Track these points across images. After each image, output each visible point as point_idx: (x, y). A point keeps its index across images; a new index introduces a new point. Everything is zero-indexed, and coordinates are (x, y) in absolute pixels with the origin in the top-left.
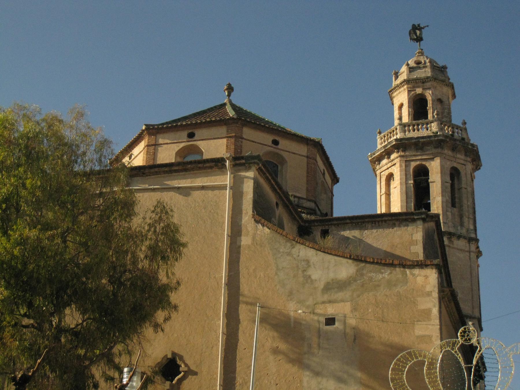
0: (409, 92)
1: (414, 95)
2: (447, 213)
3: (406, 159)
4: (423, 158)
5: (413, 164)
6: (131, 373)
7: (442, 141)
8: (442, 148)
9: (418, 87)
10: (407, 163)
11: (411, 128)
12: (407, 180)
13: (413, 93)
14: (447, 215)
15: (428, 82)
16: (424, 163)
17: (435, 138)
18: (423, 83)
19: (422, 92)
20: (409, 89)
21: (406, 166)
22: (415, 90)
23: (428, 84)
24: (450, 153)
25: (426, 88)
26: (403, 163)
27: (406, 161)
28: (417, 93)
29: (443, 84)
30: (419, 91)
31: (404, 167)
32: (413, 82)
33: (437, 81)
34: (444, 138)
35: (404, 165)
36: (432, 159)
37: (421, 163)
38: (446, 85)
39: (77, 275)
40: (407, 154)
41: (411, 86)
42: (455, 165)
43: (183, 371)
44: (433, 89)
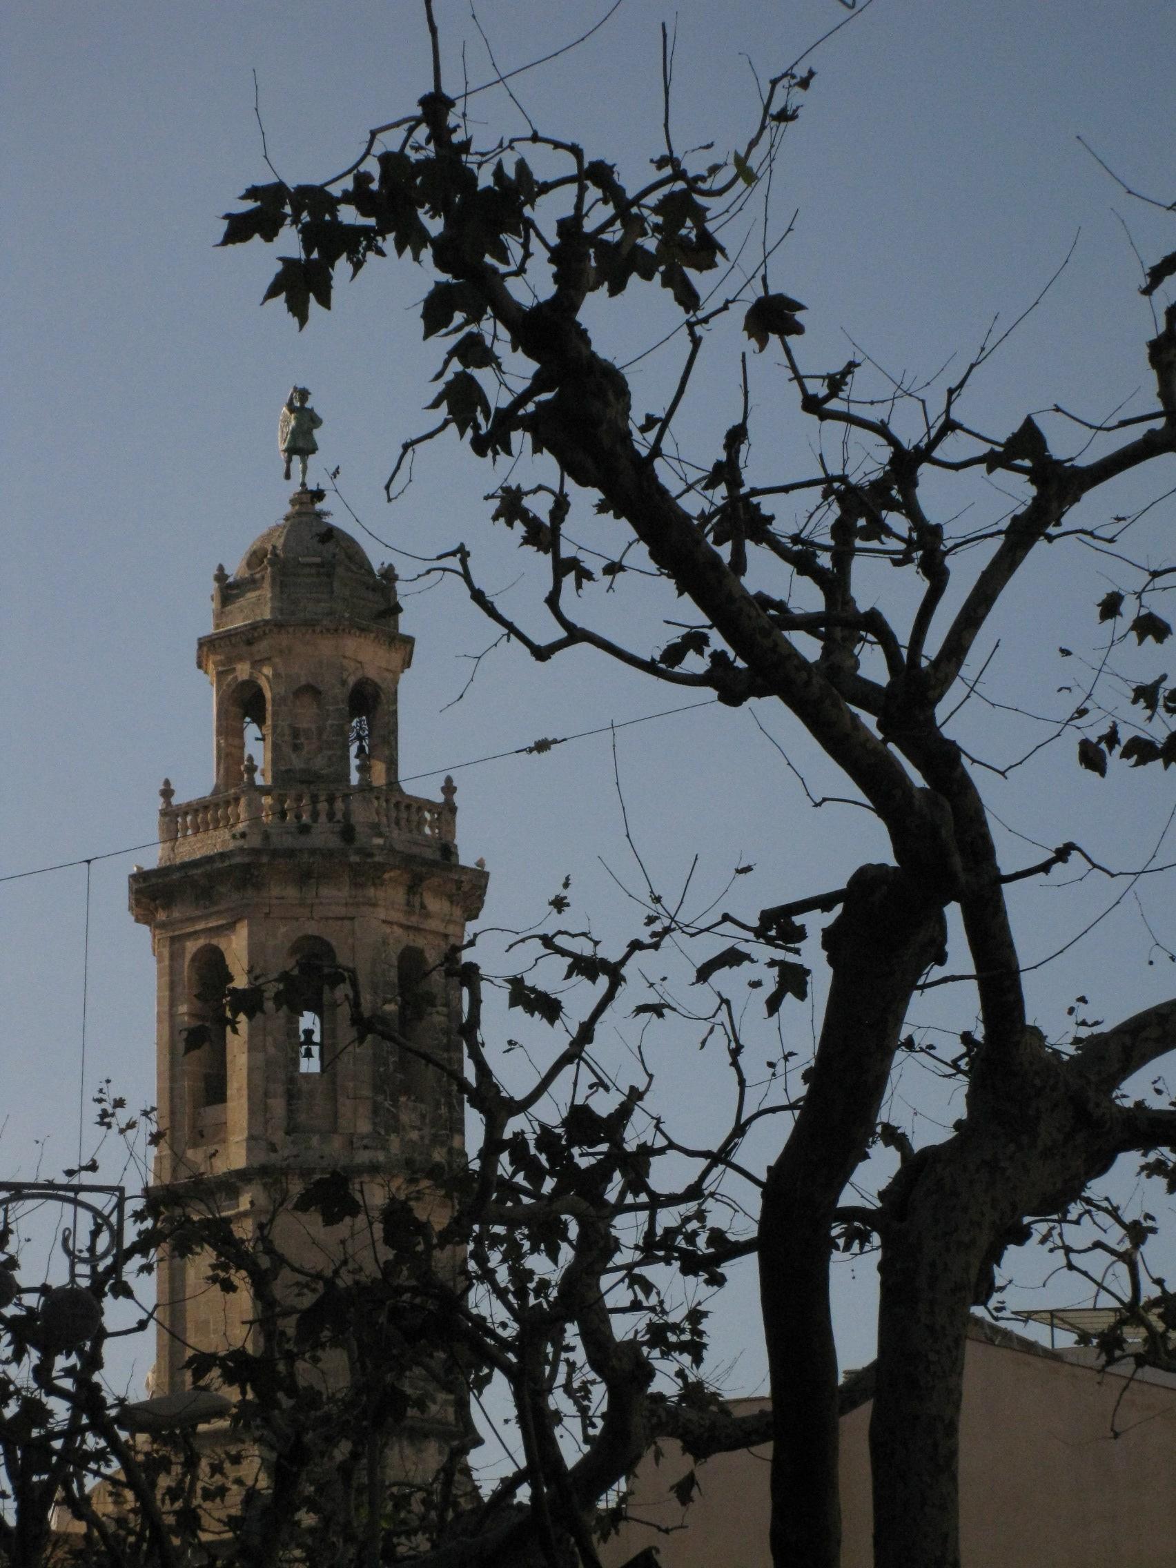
0: (220, 675)
1: (233, 687)
2: (269, 1101)
3: (171, 934)
4: (210, 925)
5: (192, 947)
6: (362, 1511)
7: (247, 868)
8: (258, 887)
9: (240, 659)
10: (177, 946)
11: (189, 818)
12: (173, 1004)
13: (230, 677)
14: (266, 1109)
15: (260, 638)
16: (214, 942)
17: (223, 862)
18: (249, 643)
19: (251, 674)
20: (220, 669)
21: (173, 957)
22: (234, 669)
23: (263, 646)
24: (291, 892)
25: (260, 661)
26: (164, 946)
27: (173, 939)
28: (240, 679)
29: (314, 631)
30: (243, 671)
31: (167, 962)
32: (222, 644)
33: (291, 630)
34: (247, 860)
35: (166, 952)
36: (231, 926)
37: (207, 942)
38: (328, 630)
39: (464, 878)
40: (176, 915)
41: (223, 658)
42: (312, 928)
43: (1095, 1336)
44: (277, 660)
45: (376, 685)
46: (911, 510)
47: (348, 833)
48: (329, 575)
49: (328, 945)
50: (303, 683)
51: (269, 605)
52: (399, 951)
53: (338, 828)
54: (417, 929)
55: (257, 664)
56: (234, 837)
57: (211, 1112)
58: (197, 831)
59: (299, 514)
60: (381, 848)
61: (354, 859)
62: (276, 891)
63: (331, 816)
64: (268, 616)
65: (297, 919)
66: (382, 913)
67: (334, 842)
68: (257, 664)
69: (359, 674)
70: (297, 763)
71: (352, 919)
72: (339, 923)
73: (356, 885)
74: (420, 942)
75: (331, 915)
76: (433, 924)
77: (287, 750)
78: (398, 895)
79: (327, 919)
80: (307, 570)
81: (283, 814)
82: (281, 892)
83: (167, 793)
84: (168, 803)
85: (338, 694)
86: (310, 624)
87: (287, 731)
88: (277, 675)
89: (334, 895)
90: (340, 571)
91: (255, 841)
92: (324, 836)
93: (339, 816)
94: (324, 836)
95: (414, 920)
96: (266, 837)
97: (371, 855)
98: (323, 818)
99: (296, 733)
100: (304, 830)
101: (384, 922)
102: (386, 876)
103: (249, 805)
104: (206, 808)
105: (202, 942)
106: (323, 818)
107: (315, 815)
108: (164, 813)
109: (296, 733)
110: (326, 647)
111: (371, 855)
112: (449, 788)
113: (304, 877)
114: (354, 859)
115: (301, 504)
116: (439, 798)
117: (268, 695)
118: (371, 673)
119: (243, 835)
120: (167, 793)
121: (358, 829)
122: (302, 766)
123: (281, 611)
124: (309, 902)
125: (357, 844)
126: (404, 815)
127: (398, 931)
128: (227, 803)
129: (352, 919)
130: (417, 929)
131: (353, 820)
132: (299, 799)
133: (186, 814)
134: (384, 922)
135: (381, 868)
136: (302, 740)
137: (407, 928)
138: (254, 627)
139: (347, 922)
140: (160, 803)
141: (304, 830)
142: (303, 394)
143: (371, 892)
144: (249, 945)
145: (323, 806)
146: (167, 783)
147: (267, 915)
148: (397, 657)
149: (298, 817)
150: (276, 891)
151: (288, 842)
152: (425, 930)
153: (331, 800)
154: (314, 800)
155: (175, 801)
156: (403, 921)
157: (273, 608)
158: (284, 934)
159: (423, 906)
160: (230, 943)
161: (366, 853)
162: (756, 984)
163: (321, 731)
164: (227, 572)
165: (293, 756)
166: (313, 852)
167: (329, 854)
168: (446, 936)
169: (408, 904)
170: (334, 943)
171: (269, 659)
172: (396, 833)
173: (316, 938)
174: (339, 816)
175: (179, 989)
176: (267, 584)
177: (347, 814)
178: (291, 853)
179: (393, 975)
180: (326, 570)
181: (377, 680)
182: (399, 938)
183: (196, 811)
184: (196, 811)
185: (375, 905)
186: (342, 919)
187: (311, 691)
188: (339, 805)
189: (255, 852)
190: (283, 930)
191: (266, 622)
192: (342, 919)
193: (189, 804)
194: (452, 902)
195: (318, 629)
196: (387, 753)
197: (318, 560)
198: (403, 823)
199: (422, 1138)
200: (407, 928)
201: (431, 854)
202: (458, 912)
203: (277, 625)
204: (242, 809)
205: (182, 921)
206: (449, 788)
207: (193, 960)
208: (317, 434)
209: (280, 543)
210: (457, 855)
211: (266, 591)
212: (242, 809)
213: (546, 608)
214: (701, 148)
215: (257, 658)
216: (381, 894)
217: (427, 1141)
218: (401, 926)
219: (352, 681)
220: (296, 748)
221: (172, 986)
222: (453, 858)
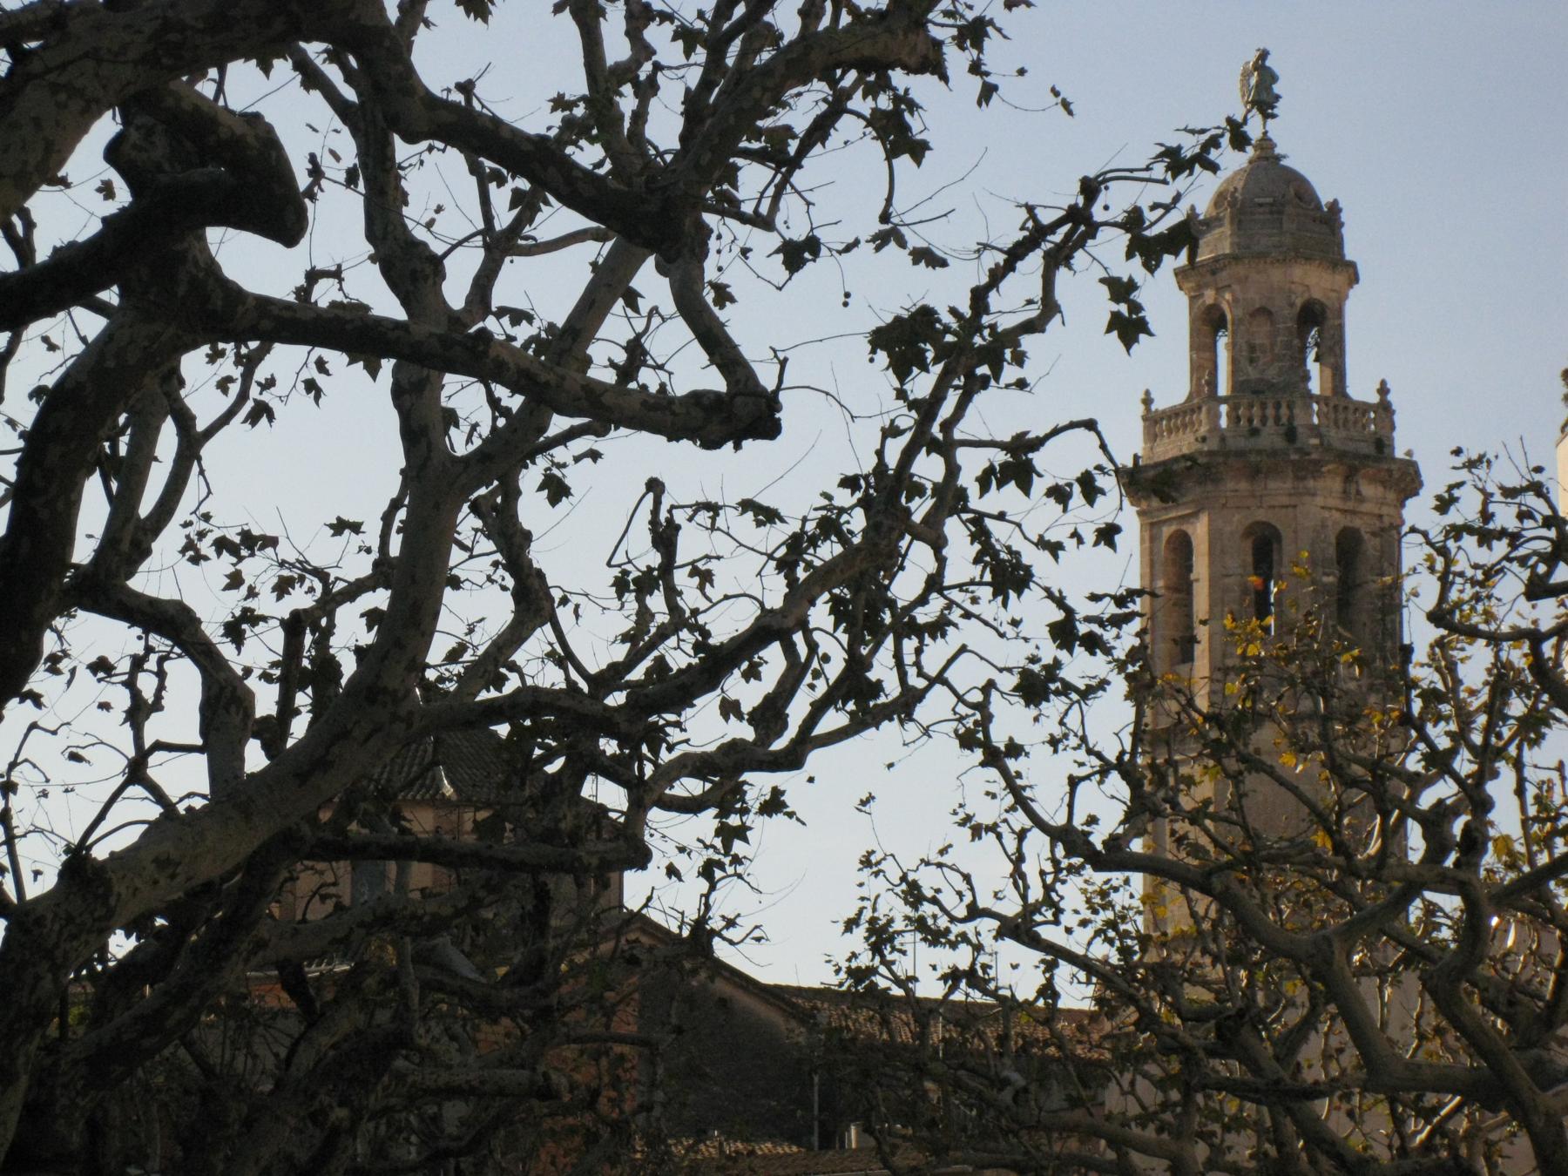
5: (1167, 531)
7: (1208, 467)
9: (1207, 286)
10: (1155, 531)
13: (1201, 301)
16: (1184, 527)
18: (1214, 273)
23: (1224, 276)
24: (1244, 486)
27: (1152, 525)
30: (1209, 296)
36: (1195, 515)
42: (1261, 515)
44: (1236, 287)
45: (1322, 304)
46: (792, 582)
47: (1291, 435)
48: (1280, 213)
49: (1274, 528)
50: (1257, 306)
51: (1229, 240)
52: (1337, 531)
53: (1282, 430)
54: (1354, 512)
55: (1219, 290)
56: (1197, 440)
57: (1183, 669)
58: (1170, 432)
59: (1259, 158)
60: (1316, 447)
61: (1294, 457)
62: (1230, 485)
63: (1277, 419)
64: (1227, 251)
65: (1248, 508)
66: (1319, 501)
67: (1280, 443)
68: (1219, 290)
69: (1306, 296)
70: (1252, 373)
71: (1295, 506)
72: (1284, 510)
73: (1299, 478)
74: (1357, 522)
75: (1276, 503)
76: (1366, 507)
77: (1244, 363)
78: (1336, 484)
79: (1274, 507)
80: (1261, 210)
81: (1238, 419)
82: (1235, 486)
83: (1147, 401)
84: (1148, 409)
85: (1287, 316)
86: (1262, 255)
87: (1245, 347)
88: (1235, 300)
89: (1279, 488)
90: (1289, 209)
91: (1213, 444)
92: (1271, 437)
93: (1284, 420)
94: (1271, 437)
95: (1350, 505)
96: (1223, 439)
97: (1308, 454)
98: (1270, 422)
99: (1252, 348)
100: (1254, 432)
101: (1323, 508)
102: (1324, 469)
103: (1209, 412)
104: (1185, 413)
105: (1173, 528)
106: (1270, 422)
107: (1264, 420)
108: (1145, 418)
109: (1252, 348)
110: (1277, 275)
111: (1308, 454)
112: (1383, 390)
113: (1254, 473)
114: (1294, 457)
115: (1262, 149)
116: (1374, 399)
117: (1229, 317)
118: (1317, 294)
119: (1204, 439)
120: (1147, 401)
121: (1300, 430)
122: (1258, 376)
123: (1238, 245)
124: (1258, 494)
125: (1298, 445)
126: (1341, 416)
127: (1337, 515)
128: (1193, 411)
129: (1295, 506)
130: (1354, 512)
131: (1296, 423)
132: (1251, 406)
133: (1162, 419)
134: (1323, 508)
135: (1318, 464)
136: (1258, 354)
137: (1344, 512)
138: (1216, 260)
139: (1290, 510)
140: (1141, 408)
141: (1254, 432)
142: (1264, 55)
143: (1311, 483)
144: (1210, 530)
145: (1270, 412)
146: (1147, 393)
147: (1224, 505)
148: (1340, 279)
149: (1250, 421)
150: (1230, 485)
151: (1241, 443)
152: (1361, 513)
153: (1278, 406)
154: (1263, 406)
155: (1153, 407)
156: (1340, 504)
157: (1232, 244)
158: (1237, 521)
159: (1358, 492)
160: (1195, 529)
161: (1303, 452)
162: (37, 873)
163: (1273, 345)
164: (1198, 211)
165: (1250, 369)
166: (1259, 452)
167: (1274, 453)
168: (1380, 516)
169: (1345, 492)
170: (1279, 527)
171: (1229, 286)
172: (1333, 433)
173: (1264, 523)
174: (1284, 420)
175: (1157, 567)
176: (1227, 221)
177: (1291, 418)
178: (1240, 454)
179: (1332, 552)
180: (1276, 209)
181: (1323, 300)
182: (1338, 520)
183: (1169, 418)
184: (1169, 418)
185: (1314, 495)
186: (1287, 507)
187: (1264, 312)
188: (1284, 411)
189: (1211, 453)
190: (1237, 518)
191: (1225, 256)
192: (1287, 507)
193: (1164, 412)
194: (1385, 487)
195: (1268, 260)
196: (1332, 360)
197: (1269, 200)
198: (1341, 422)
199: (1360, 686)
200: (1344, 512)
201: (1367, 449)
202: (1391, 496)
203: (1235, 258)
204: (1203, 415)
205: (1158, 510)
206: (1383, 390)
207: (1168, 542)
208: (1277, 88)
209: (1240, 185)
210: (1393, 449)
211: (1227, 229)
212: (1203, 415)
213: (1085, 417)
214: (1185, 130)
215: (1220, 285)
216: (1320, 484)
217: (1364, 689)
218: (1338, 510)
219: (1299, 302)
220: (1252, 361)
221: (1152, 564)
222: (1386, 451)
